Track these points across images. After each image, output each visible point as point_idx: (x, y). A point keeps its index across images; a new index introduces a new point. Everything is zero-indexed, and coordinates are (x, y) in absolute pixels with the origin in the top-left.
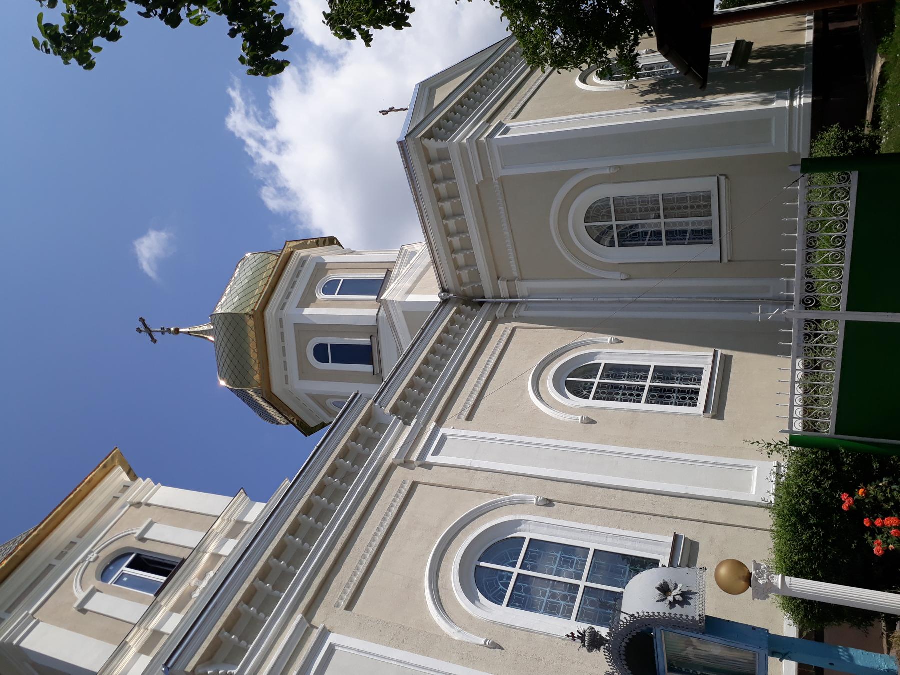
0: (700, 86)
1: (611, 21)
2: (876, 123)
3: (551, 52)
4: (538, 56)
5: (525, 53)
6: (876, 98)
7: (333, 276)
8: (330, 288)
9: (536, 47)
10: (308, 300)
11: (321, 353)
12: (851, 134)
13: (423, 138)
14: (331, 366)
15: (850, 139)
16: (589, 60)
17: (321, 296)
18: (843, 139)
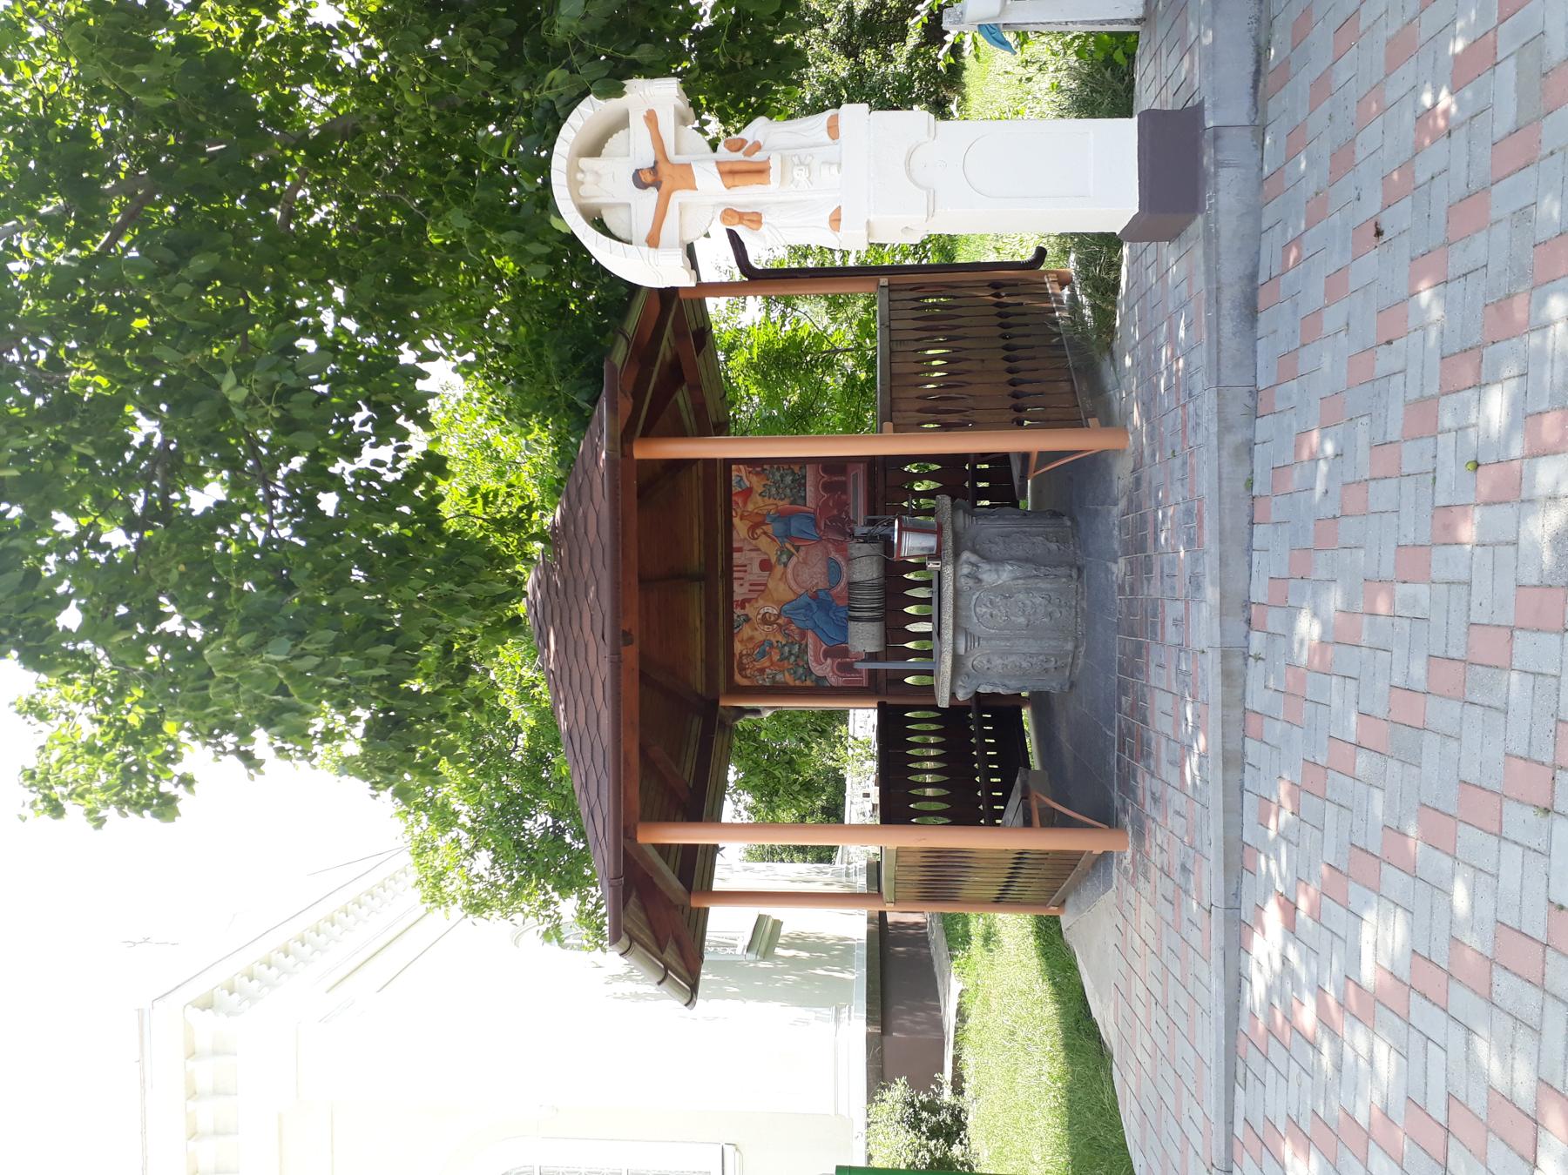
0: (686, 1001)
1: (571, 852)
2: (958, 1090)
3: (465, 887)
4: (440, 890)
5: (419, 883)
6: (956, 1043)
9: (440, 876)
12: (925, 1098)
13: (189, 1007)
15: (924, 1107)
16: (527, 909)
18: (912, 1105)
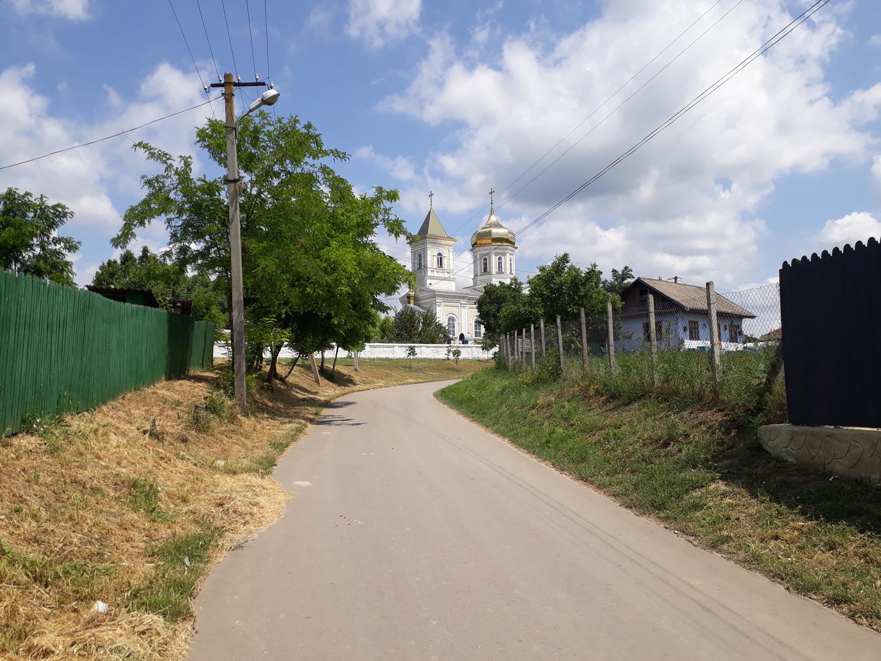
7: (503, 258)
8: (500, 259)
10: (496, 254)
11: (485, 259)
14: (483, 262)
17: (498, 257)
